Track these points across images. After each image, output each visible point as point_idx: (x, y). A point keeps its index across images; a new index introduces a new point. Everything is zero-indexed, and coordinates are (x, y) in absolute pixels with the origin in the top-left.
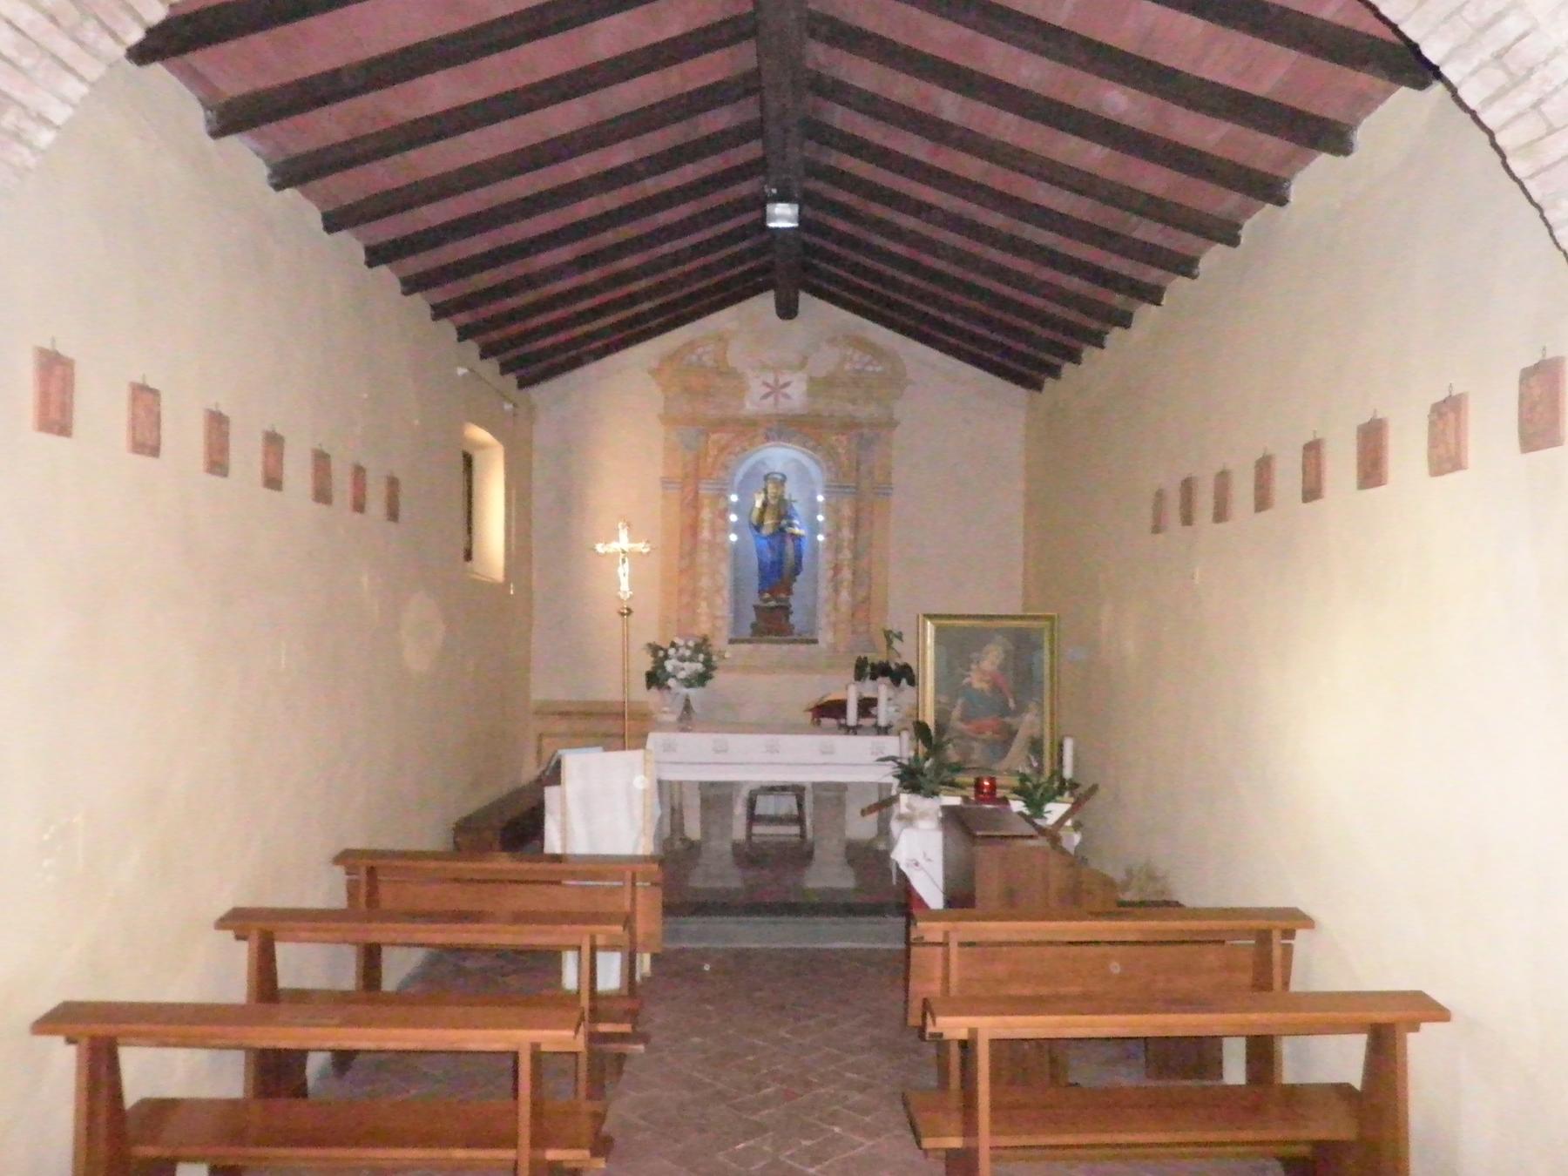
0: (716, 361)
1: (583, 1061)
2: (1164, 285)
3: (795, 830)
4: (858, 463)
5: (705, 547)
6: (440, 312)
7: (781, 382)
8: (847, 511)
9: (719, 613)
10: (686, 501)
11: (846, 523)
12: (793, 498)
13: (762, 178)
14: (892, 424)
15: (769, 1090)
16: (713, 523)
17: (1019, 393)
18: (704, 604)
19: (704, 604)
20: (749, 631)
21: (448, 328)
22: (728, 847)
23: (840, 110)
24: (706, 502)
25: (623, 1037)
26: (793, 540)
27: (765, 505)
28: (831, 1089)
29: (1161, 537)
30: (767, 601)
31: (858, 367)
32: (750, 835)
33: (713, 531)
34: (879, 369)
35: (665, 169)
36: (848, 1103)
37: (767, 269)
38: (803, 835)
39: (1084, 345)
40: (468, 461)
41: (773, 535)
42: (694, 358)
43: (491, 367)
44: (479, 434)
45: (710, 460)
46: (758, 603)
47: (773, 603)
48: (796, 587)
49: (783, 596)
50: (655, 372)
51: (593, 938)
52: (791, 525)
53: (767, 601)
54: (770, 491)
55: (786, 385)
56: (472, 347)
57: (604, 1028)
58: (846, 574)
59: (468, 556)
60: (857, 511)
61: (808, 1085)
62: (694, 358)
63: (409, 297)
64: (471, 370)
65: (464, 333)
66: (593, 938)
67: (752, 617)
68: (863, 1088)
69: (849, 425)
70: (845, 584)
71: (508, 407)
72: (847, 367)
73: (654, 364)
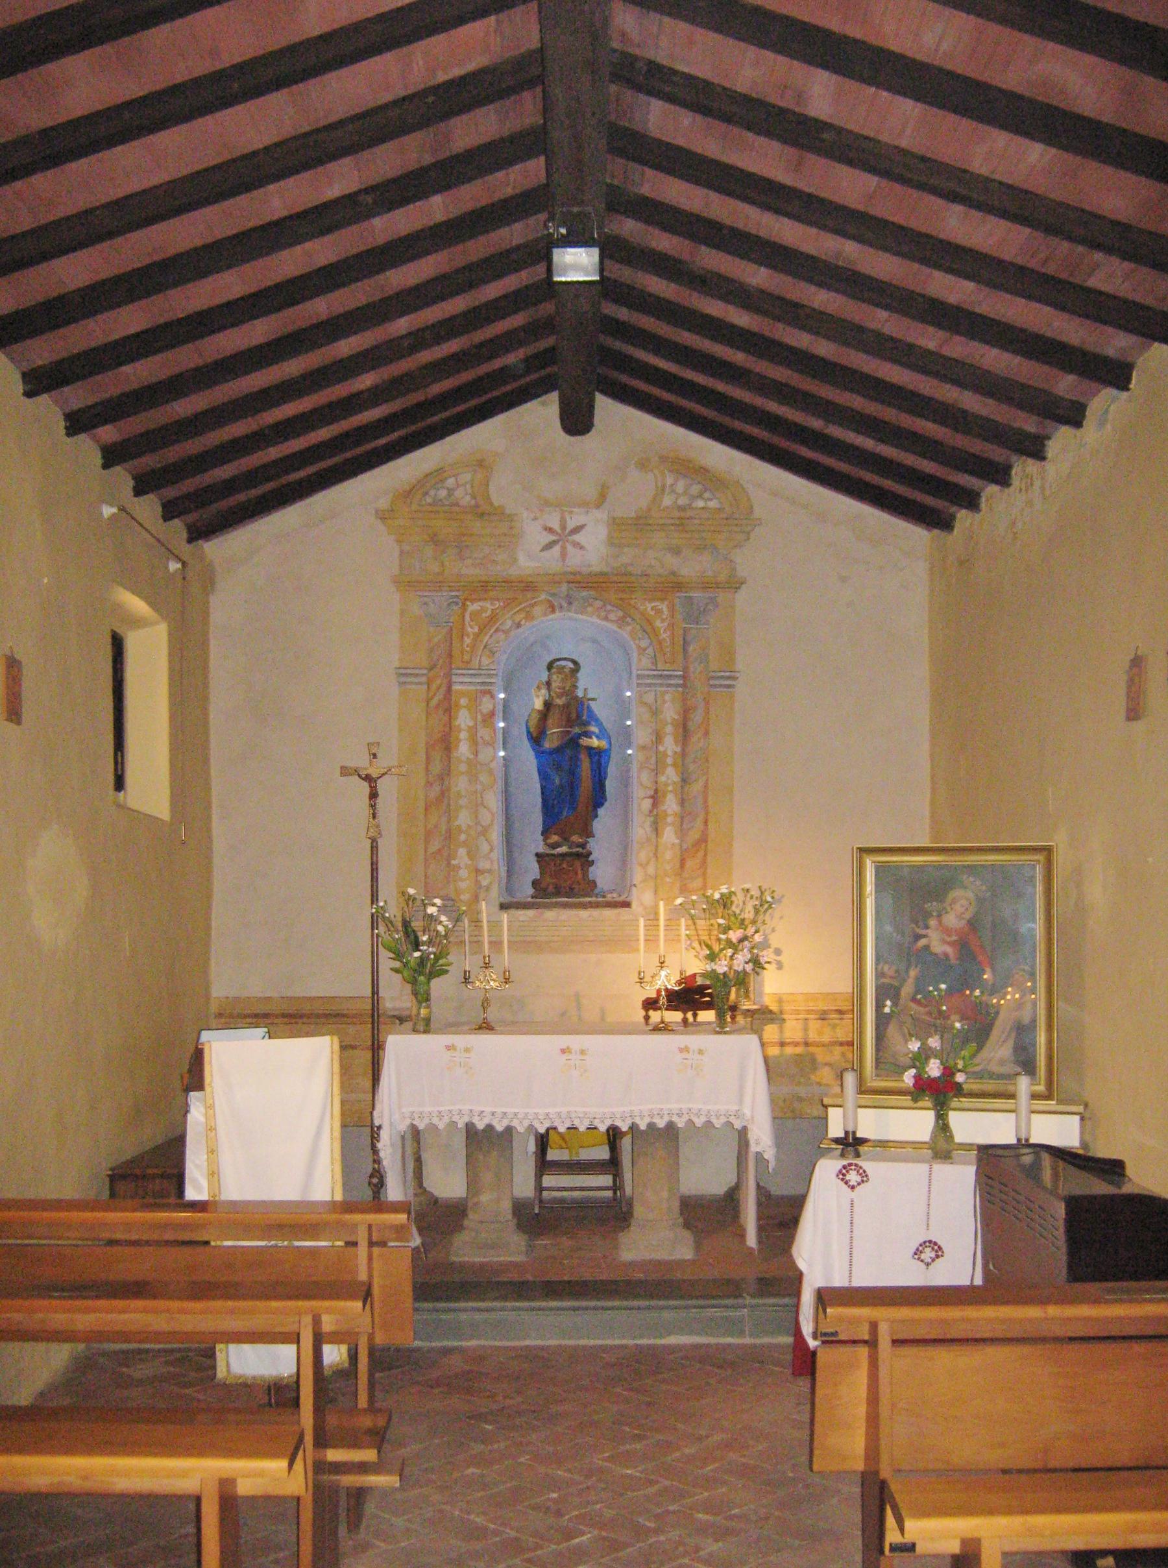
0: (474, 497)
1: (307, 1515)
2: (1129, 359)
3: (606, 1180)
4: (686, 644)
5: (463, 768)
6: (77, 423)
7: (571, 525)
8: (670, 713)
9: (484, 865)
10: (434, 702)
11: (669, 729)
12: (590, 696)
13: (542, 216)
14: (735, 584)
15: (584, 1538)
16: (473, 731)
17: (916, 535)
18: (462, 852)
19: (462, 852)
20: (531, 891)
21: (87, 449)
22: (507, 1206)
23: (657, 107)
24: (463, 701)
25: (362, 1468)
26: (590, 756)
27: (548, 705)
28: (674, 1534)
29: (1139, 726)
30: (554, 846)
31: (683, 501)
32: (540, 1189)
33: (474, 742)
34: (713, 504)
35: (404, 201)
36: (702, 1553)
37: (547, 357)
38: (616, 1187)
39: (1014, 458)
40: (118, 645)
41: (558, 750)
42: (443, 493)
43: (148, 507)
44: (137, 605)
45: (467, 641)
46: (542, 849)
47: (564, 849)
48: (598, 826)
49: (575, 838)
50: (384, 516)
51: (317, 1321)
52: (588, 734)
53: (554, 846)
54: (554, 685)
55: (577, 530)
56: (122, 478)
57: (334, 1455)
58: (671, 804)
59: (119, 783)
60: (686, 713)
61: (640, 1532)
62: (443, 493)
63: (31, 400)
64: (122, 509)
65: (112, 456)
66: (317, 1321)
67: (533, 870)
68: (722, 1534)
69: (673, 586)
70: (669, 819)
71: (174, 566)
72: (667, 501)
73: (383, 503)
